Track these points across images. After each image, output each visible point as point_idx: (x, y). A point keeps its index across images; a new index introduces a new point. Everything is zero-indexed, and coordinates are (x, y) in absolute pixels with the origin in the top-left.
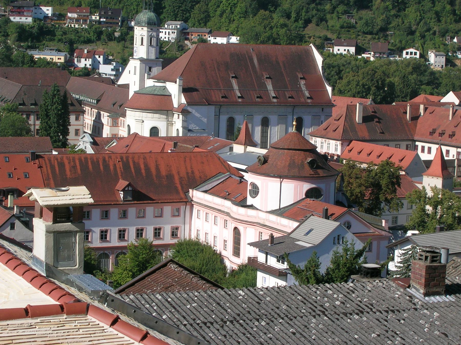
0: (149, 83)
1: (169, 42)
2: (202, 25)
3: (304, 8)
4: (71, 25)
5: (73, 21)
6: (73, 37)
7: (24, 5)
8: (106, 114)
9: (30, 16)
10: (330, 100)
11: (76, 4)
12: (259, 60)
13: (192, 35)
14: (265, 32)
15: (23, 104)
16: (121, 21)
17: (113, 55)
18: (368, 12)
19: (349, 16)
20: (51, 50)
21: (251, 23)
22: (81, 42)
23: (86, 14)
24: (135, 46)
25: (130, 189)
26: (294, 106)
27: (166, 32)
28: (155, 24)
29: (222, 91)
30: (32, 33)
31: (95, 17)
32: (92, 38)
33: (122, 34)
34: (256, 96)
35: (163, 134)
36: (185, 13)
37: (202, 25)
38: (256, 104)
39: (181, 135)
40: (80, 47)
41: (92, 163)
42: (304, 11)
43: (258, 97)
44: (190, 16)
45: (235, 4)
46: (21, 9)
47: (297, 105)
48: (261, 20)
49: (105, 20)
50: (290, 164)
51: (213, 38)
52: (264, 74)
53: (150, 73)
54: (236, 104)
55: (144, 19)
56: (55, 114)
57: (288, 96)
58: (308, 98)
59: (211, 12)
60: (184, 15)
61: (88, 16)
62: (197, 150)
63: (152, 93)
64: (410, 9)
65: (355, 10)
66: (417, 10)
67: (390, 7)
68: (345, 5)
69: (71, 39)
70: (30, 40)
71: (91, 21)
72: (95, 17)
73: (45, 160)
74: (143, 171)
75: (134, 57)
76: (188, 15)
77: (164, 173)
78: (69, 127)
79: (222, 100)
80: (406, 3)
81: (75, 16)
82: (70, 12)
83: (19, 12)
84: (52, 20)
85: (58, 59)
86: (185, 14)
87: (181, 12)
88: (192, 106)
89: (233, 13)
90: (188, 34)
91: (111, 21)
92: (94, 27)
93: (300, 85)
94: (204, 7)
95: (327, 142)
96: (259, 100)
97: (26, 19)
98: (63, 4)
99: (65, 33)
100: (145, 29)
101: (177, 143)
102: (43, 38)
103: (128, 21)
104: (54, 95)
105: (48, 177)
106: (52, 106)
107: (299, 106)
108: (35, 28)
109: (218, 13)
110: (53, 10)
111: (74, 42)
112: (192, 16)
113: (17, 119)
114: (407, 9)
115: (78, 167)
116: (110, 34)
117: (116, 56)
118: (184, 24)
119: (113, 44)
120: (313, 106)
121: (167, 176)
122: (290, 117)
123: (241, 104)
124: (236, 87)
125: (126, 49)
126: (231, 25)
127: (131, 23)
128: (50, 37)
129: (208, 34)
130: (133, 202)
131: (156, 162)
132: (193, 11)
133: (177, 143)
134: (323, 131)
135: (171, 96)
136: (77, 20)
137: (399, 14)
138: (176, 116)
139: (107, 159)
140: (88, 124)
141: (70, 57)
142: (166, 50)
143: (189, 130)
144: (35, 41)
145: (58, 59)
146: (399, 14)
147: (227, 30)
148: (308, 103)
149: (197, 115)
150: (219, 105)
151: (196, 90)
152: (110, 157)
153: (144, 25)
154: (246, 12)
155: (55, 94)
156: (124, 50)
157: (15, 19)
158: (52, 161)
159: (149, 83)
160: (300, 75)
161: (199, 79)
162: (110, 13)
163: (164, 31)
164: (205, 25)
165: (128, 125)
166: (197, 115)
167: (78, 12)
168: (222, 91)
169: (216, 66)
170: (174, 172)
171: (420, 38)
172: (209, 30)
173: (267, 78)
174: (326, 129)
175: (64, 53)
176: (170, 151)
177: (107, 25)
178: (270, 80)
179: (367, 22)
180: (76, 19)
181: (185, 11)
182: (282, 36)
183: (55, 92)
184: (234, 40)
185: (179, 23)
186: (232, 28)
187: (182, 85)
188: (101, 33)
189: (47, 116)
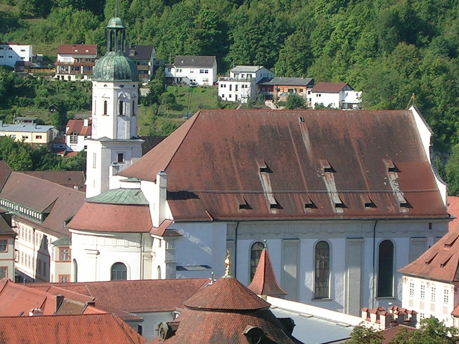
0: (115, 182)
1: (237, 102)
4: (63, 77)
5: (67, 70)
6: (65, 97)
10: (445, 209)
11: (75, 39)
12: (314, 138)
13: (279, 90)
14: (407, 83)
16: (151, 68)
20: (26, 121)
21: (386, 66)
22: (81, 107)
23: (91, 57)
26: (377, 220)
27: (231, 86)
28: (128, 77)
29: (242, 195)
33: (152, 89)
34: (304, 203)
35: (133, 275)
37: (299, 71)
39: (163, 277)
40: (77, 116)
43: (307, 206)
45: (356, 33)
47: (381, 219)
50: (212, 337)
51: (315, 94)
52: (321, 162)
53: (118, 164)
54: (268, 218)
55: (109, 68)
57: (364, 202)
58: (402, 205)
59: (314, 49)
60: (267, 55)
61: (93, 60)
62: (91, 310)
75: (93, 137)
79: (240, 211)
81: (71, 60)
82: (62, 54)
84: (30, 68)
85: (37, 137)
86: (269, 53)
87: (261, 49)
89: (352, 49)
93: (387, 181)
95: (430, 286)
96: (309, 210)
98: (52, 39)
100: (111, 85)
101: (63, 297)
103: (165, 67)
107: (385, 219)
109: (327, 49)
110: (34, 51)
111: (68, 106)
112: (281, 55)
118: (266, 71)
120: (412, 219)
123: (276, 218)
124: (267, 187)
125: (159, 118)
126: (349, 71)
127: (170, 71)
128: (24, 98)
129: (307, 87)
133: (63, 297)
134: (425, 266)
135: (148, 205)
136: (75, 68)
138: (156, 242)
140: (29, 258)
141: (59, 134)
143: (179, 268)
145: (37, 137)
147: (342, 80)
148: (402, 214)
149: (193, 239)
150: (235, 222)
151: (193, 196)
154: (376, 46)
160: (389, 164)
161: (199, 175)
163: (228, 84)
164: (305, 72)
165: (75, 260)
168: (242, 195)
169: (231, 151)
172: (309, 80)
173: (326, 170)
174: (430, 262)
175: (47, 128)
176: (31, 314)
178: (332, 174)
180: (72, 66)
181: (268, 47)
182: (438, 89)
184: (352, 97)
185: (256, 68)
186: (350, 77)
187: (165, 185)
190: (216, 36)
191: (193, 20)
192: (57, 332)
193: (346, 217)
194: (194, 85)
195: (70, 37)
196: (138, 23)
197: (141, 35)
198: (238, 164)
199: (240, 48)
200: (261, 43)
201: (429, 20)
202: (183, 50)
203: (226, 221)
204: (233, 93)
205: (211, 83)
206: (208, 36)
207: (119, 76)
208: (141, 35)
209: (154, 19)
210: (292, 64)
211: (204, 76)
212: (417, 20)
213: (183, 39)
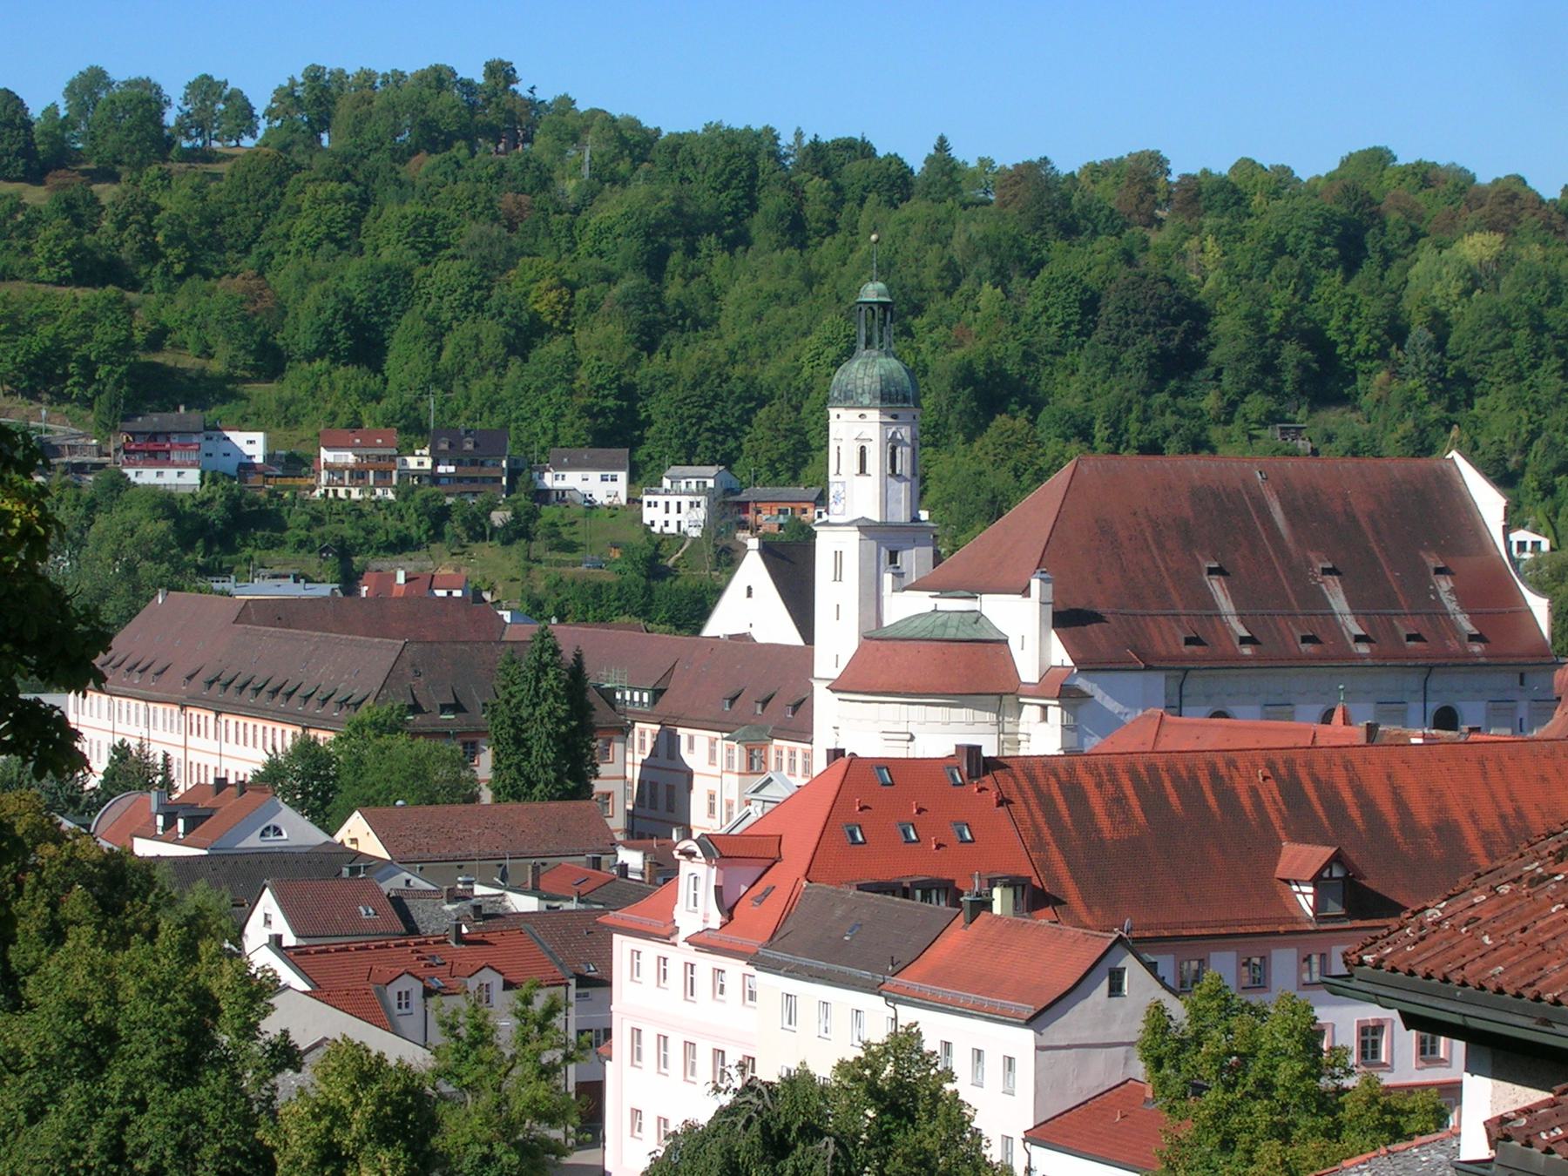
1: (680, 537)
2: (785, 477)
3: (1135, 407)
4: (335, 492)
5: (342, 478)
6: (347, 531)
7: (169, 429)
8: (702, 737)
9: (193, 465)
11: (342, 419)
13: (759, 512)
15: (416, 708)
17: (492, 589)
18: (1348, 416)
19: (1284, 431)
20: (275, 577)
22: (378, 549)
23: (388, 452)
24: (832, 478)
25: (1337, 873)
28: (906, 399)
29: (1183, 618)
30: (206, 521)
31: (419, 461)
32: (414, 532)
33: (516, 514)
36: (720, 438)
37: (785, 477)
38: (1302, 662)
41: (1175, 786)
42: (1133, 416)
43: (1305, 640)
44: (739, 448)
46: (161, 440)
47: (1438, 666)
48: (1002, 449)
49: (452, 469)
52: (1312, 556)
54: (1233, 664)
56: (549, 735)
57: (1403, 633)
61: (392, 458)
63: (938, 634)
64: (1489, 401)
65: (1304, 410)
66: (1516, 403)
67: (1423, 394)
68: (1268, 393)
69: (343, 540)
70: (200, 543)
71: (405, 475)
72: (419, 461)
73: (1014, 777)
74: (1354, 812)
76: (732, 443)
77: (1424, 818)
78: (593, 782)
79: (1188, 650)
80: (1474, 382)
81: (349, 458)
83: (154, 450)
86: (723, 443)
88: (1091, 675)
90: (744, 507)
91: (473, 472)
92: (417, 497)
93: (1436, 593)
94: (788, 418)
96: (1307, 648)
97: (179, 474)
98: (296, 422)
99: (317, 520)
100: (874, 415)
101: (1376, 726)
102: (244, 539)
104: (542, 668)
105: (1041, 839)
106: (535, 705)
107: (1445, 665)
108: (217, 505)
110: (269, 443)
111: (352, 547)
112: (746, 446)
113: (429, 754)
114: (1478, 402)
115: (1134, 801)
116: (475, 517)
117: (505, 590)
119: (487, 552)
121: (1436, 828)
122: (1415, 707)
124: (1225, 604)
127: (541, 477)
130: (1348, 924)
131: (1389, 777)
132: (748, 429)
135: (1006, 642)
136: (358, 474)
137: (1453, 416)
139: (1223, 771)
142: (675, 566)
144: (217, 549)
146: (1453, 416)
148: (1474, 655)
149: (1112, 706)
151: (1096, 618)
152: (1231, 764)
153: (866, 402)
155: (547, 665)
156: (529, 569)
157: (146, 476)
158: (1042, 781)
159: (902, 606)
160: (1433, 561)
162: (469, 447)
163: (661, 500)
166: (1112, 706)
167: (358, 446)
170: (1459, 814)
171: (1539, 496)
173: (1325, 571)
177: (462, 487)
179: (1356, 445)
180: (352, 471)
183: (546, 657)
185: (713, 470)
188: (444, 513)
189: (519, 742)
190: (619, 412)
191: (572, 382)
192: (1484, 774)
193: (1377, 662)
194: (591, 506)
195: (333, 416)
196: (458, 390)
197: (467, 413)
198: (1164, 560)
199: (667, 434)
200: (707, 424)
201: (1023, 377)
202: (556, 439)
203: (1161, 669)
204: (673, 517)
205: (623, 499)
206: (602, 412)
207: (891, 399)
208: (467, 413)
209: (489, 380)
210: (771, 464)
211: (609, 485)
212: (1002, 373)
213: (556, 418)
